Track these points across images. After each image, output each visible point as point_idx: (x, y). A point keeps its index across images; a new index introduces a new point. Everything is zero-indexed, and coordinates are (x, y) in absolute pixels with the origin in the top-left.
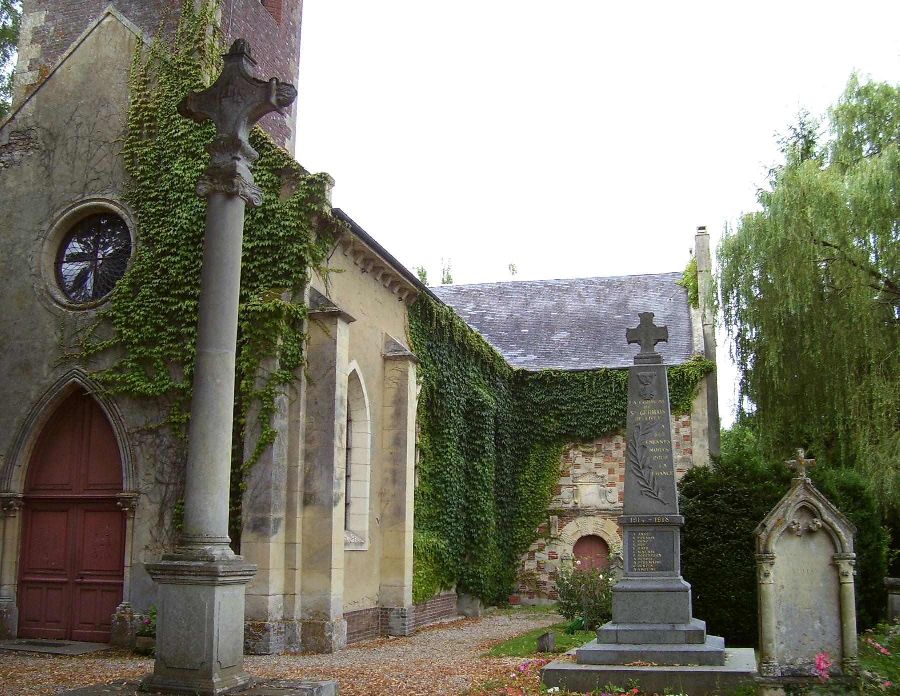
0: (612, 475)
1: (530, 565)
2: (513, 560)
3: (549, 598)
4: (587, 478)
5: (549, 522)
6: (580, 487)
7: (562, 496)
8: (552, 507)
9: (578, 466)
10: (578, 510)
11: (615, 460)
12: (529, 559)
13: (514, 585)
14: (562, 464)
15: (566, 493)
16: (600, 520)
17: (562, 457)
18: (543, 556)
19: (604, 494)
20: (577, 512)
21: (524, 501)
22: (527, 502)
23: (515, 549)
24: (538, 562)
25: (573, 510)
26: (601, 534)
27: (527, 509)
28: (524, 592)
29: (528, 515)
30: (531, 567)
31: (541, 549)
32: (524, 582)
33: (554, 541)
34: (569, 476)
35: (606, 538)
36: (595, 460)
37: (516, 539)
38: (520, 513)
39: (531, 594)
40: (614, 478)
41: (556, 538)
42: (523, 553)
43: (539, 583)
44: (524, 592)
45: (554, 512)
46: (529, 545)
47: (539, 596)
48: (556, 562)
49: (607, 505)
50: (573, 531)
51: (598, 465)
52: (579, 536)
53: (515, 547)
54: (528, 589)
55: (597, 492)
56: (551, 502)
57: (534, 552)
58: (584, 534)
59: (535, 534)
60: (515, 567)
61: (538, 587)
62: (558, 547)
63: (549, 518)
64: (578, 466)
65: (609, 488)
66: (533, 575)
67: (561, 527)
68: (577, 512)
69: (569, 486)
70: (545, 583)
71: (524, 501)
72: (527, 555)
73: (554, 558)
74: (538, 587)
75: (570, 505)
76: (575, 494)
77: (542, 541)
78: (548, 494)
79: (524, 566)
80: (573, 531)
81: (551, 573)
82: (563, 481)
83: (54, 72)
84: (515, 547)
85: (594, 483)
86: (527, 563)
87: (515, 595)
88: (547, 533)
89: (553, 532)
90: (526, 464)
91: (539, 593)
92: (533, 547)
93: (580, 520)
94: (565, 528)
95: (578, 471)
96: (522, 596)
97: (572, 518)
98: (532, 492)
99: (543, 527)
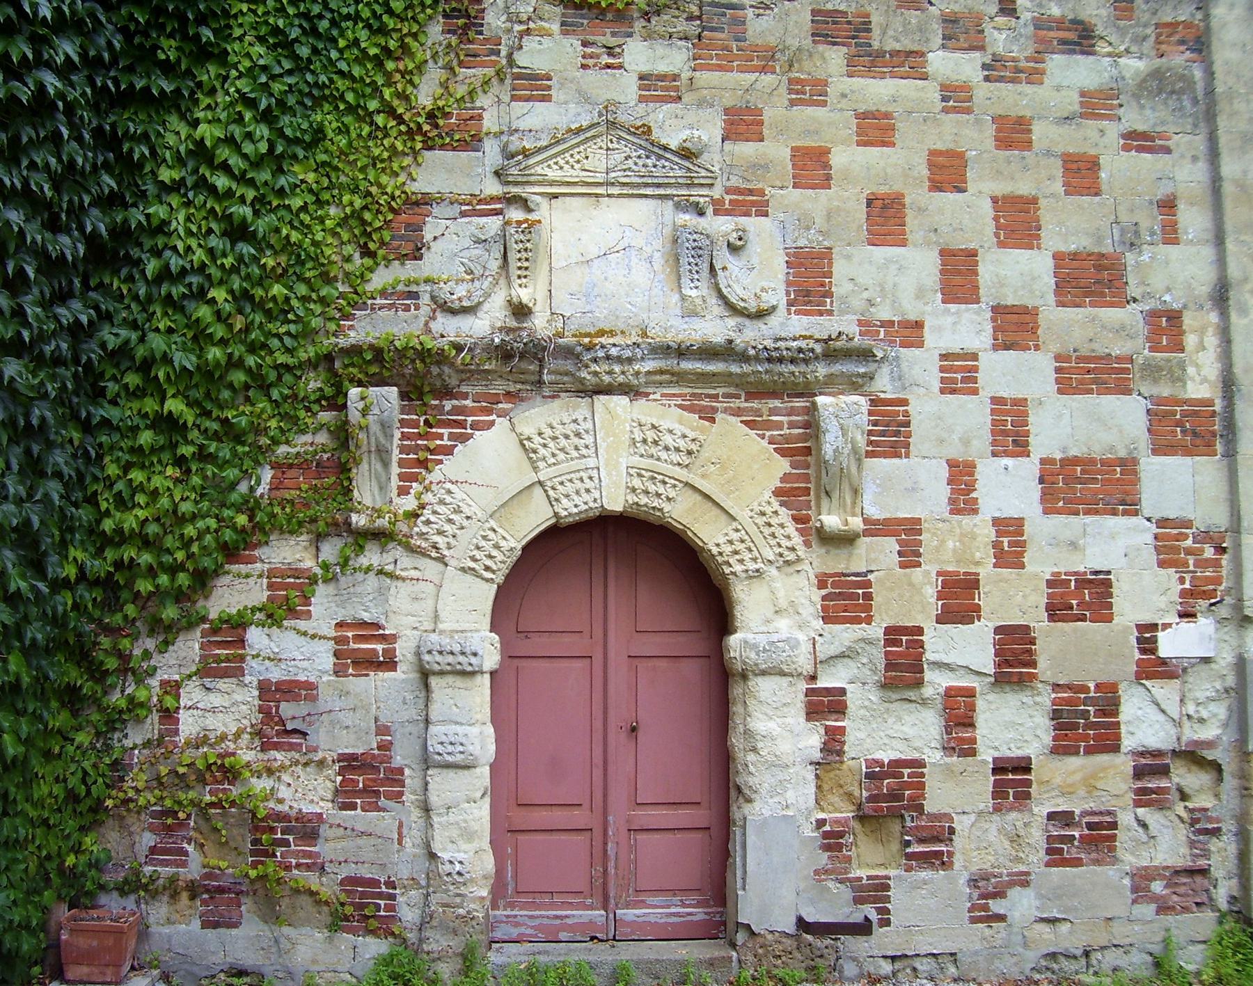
0: (746, 150)
1: (215, 713)
2: (99, 674)
3: (339, 921)
4: (598, 159)
5: (343, 435)
6: (544, 210)
7: (431, 264)
8: (363, 330)
9: (534, 87)
10: (535, 351)
11: (765, 59)
12: (209, 671)
13: (108, 842)
14: (435, 74)
15: (450, 248)
16: (665, 415)
17: (435, 32)
18: (298, 651)
19: (691, 258)
20: (529, 364)
21: (180, 291)
22: (200, 295)
23: (112, 603)
24: (265, 689)
25: (505, 353)
26: (680, 511)
27: (201, 337)
28: (173, 889)
29: (208, 379)
30: (222, 724)
31: (285, 605)
32: (168, 822)
33: (372, 556)
34: (472, 143)
35: (710, 534)
36: (640, 55)
37: (120, 538)
38: (146, 367)
39: (217, 900)
40: (761, 167)
41: (381, 537)
42: (167, 632)
43: (270, 832)
44: (173, 889)
45: (379, 364)
46: (203, 580)
47: (271, 914)
48: (385, 691)
49: (714, 328)
50: (500, 478)
51: (657, 87)
52: (534, 518)
53: (112, 589)
54: (194, 868)
55: (657, 247)
56: (358, 300)
57: (235, 627)
58: (573, 506)
59: (250, 506)
60: (115, 721)
61: (262, 853)
62: (400, 596)
63: (337, 402)
64: (534, 87)
65: (723, 226)
66: (231, 774)
67: (421, 463)
68: (529, 364)
69: (474, 206)
70: (308, 828)
71: (180, 291)
72: (190, 647)
73: (368, 663)
74: (262, 853)
75: (485, 324)
76: (516, 253)
77: (288, 552)
78: (340, 253)
79: (169, 716)
80: (500, 478)
81: (350, 763)
82: (436, 173)
83: (606, 586)
84: (112, 589)
85: (634, 190)
86: (192, 694)
87: (112, 903)
88: (325, 505)
89: (365, 492)
90: (204, 54)
91: (272, 897)
92: (235, 593)
93: (537, 417)
94: (449, 468)
95: (537, 118)
96: (157, 912)
97: (490, 404)
98: (238, 232)
99: (301, 463)
